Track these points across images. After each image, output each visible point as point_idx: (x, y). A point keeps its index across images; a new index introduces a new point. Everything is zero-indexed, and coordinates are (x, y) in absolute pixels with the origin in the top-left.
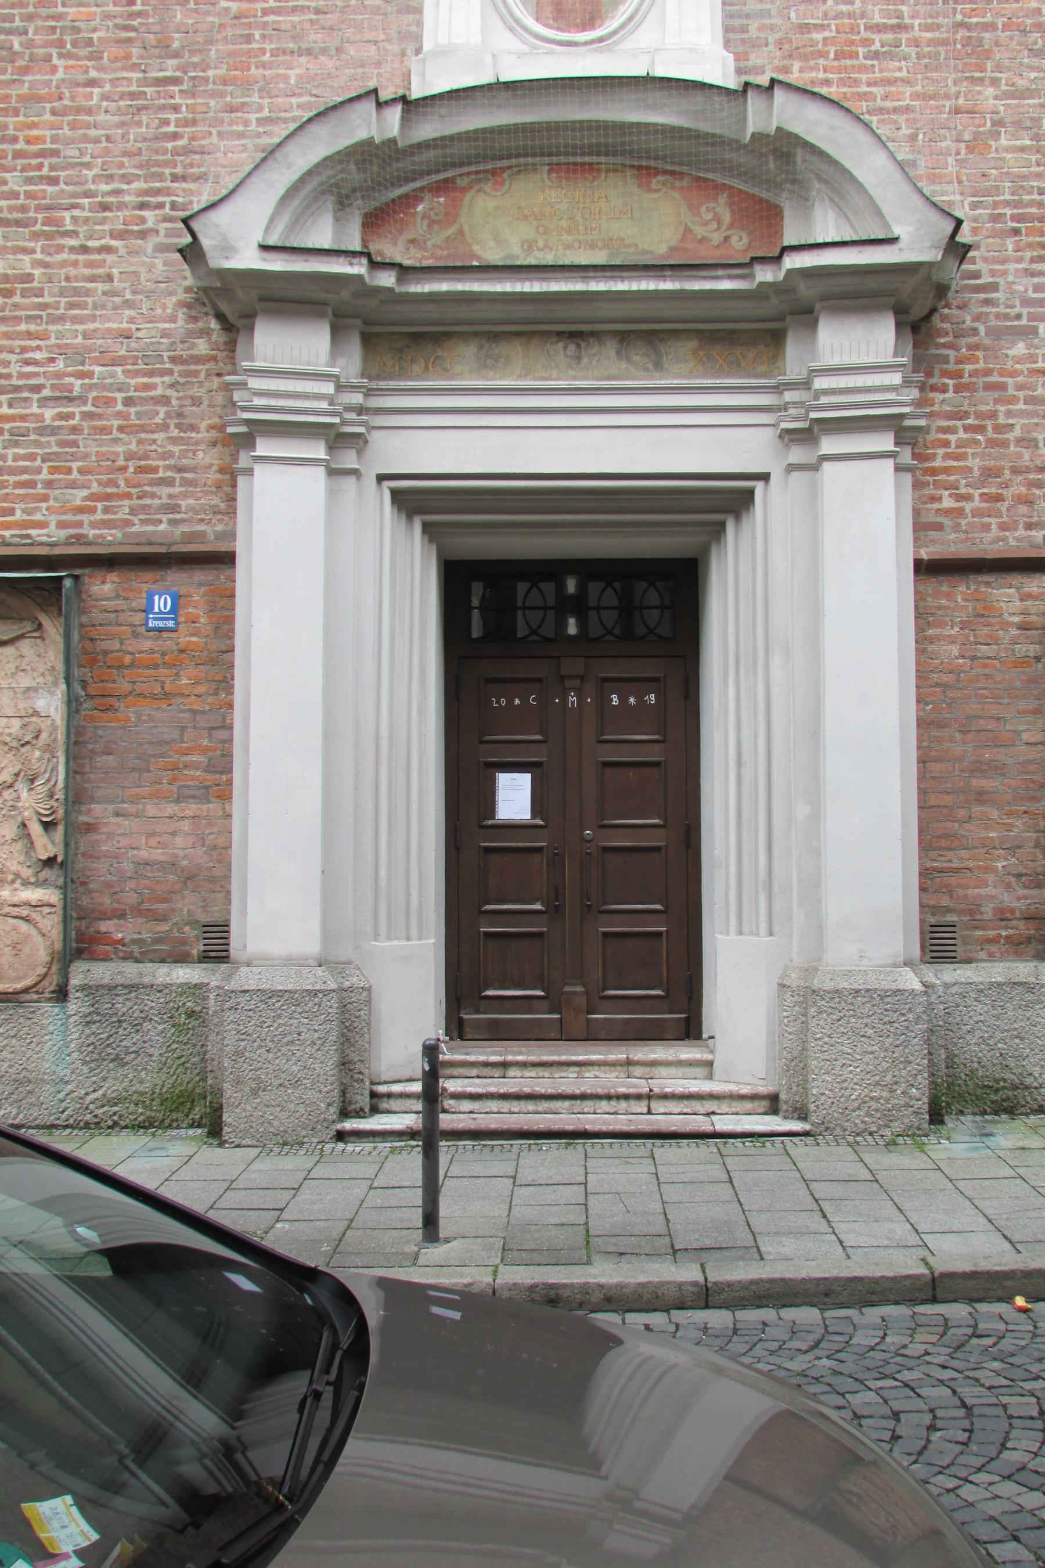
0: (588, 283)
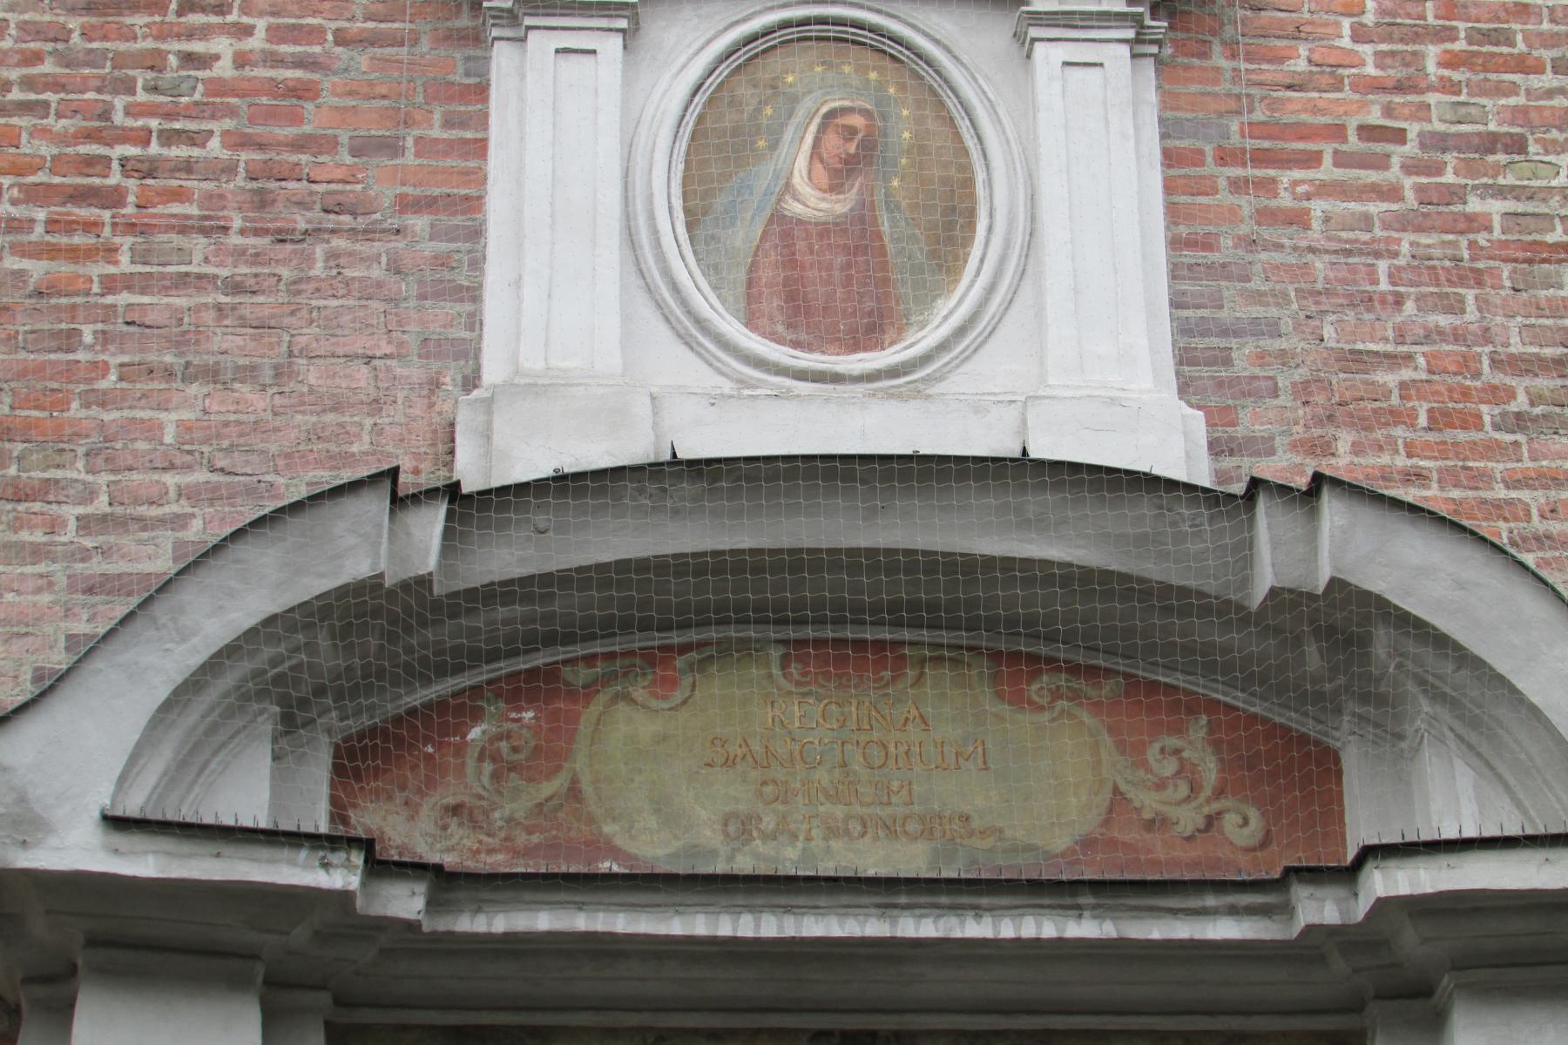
0: (894, 921)
